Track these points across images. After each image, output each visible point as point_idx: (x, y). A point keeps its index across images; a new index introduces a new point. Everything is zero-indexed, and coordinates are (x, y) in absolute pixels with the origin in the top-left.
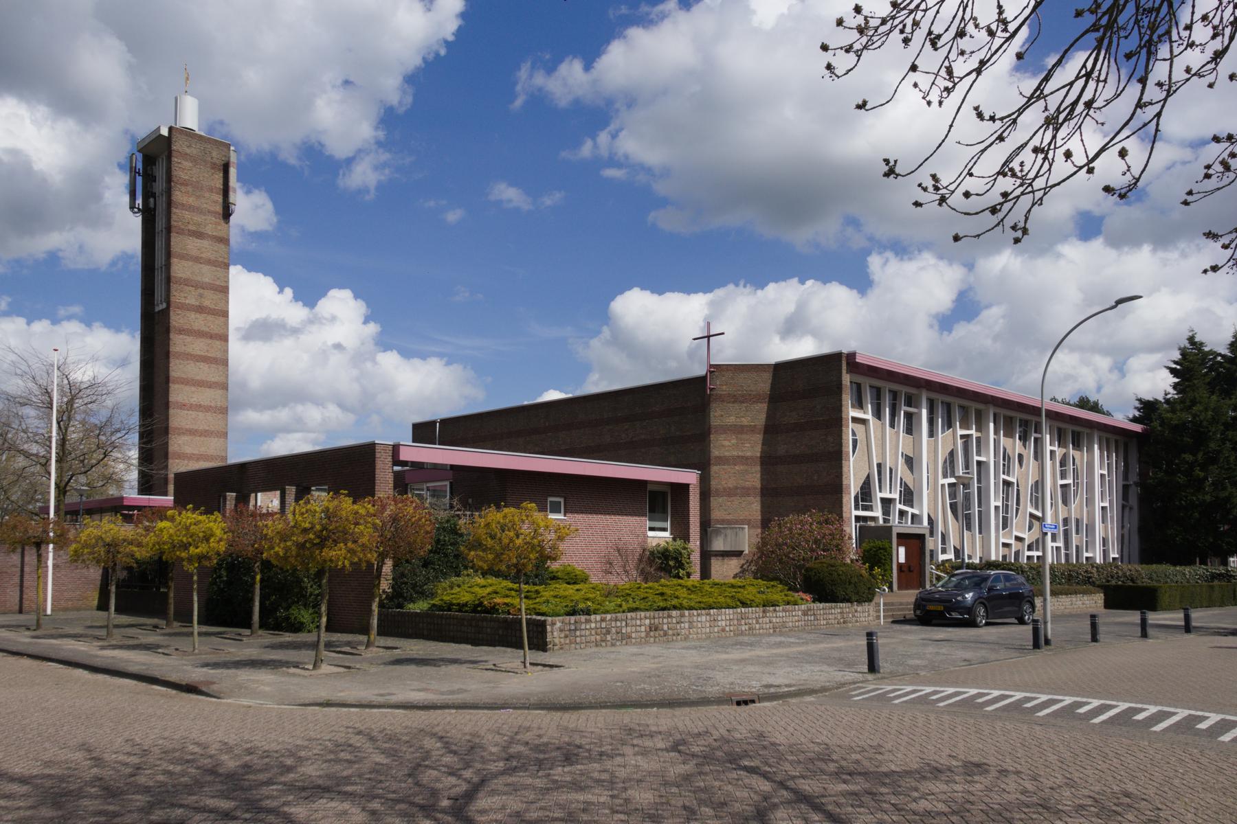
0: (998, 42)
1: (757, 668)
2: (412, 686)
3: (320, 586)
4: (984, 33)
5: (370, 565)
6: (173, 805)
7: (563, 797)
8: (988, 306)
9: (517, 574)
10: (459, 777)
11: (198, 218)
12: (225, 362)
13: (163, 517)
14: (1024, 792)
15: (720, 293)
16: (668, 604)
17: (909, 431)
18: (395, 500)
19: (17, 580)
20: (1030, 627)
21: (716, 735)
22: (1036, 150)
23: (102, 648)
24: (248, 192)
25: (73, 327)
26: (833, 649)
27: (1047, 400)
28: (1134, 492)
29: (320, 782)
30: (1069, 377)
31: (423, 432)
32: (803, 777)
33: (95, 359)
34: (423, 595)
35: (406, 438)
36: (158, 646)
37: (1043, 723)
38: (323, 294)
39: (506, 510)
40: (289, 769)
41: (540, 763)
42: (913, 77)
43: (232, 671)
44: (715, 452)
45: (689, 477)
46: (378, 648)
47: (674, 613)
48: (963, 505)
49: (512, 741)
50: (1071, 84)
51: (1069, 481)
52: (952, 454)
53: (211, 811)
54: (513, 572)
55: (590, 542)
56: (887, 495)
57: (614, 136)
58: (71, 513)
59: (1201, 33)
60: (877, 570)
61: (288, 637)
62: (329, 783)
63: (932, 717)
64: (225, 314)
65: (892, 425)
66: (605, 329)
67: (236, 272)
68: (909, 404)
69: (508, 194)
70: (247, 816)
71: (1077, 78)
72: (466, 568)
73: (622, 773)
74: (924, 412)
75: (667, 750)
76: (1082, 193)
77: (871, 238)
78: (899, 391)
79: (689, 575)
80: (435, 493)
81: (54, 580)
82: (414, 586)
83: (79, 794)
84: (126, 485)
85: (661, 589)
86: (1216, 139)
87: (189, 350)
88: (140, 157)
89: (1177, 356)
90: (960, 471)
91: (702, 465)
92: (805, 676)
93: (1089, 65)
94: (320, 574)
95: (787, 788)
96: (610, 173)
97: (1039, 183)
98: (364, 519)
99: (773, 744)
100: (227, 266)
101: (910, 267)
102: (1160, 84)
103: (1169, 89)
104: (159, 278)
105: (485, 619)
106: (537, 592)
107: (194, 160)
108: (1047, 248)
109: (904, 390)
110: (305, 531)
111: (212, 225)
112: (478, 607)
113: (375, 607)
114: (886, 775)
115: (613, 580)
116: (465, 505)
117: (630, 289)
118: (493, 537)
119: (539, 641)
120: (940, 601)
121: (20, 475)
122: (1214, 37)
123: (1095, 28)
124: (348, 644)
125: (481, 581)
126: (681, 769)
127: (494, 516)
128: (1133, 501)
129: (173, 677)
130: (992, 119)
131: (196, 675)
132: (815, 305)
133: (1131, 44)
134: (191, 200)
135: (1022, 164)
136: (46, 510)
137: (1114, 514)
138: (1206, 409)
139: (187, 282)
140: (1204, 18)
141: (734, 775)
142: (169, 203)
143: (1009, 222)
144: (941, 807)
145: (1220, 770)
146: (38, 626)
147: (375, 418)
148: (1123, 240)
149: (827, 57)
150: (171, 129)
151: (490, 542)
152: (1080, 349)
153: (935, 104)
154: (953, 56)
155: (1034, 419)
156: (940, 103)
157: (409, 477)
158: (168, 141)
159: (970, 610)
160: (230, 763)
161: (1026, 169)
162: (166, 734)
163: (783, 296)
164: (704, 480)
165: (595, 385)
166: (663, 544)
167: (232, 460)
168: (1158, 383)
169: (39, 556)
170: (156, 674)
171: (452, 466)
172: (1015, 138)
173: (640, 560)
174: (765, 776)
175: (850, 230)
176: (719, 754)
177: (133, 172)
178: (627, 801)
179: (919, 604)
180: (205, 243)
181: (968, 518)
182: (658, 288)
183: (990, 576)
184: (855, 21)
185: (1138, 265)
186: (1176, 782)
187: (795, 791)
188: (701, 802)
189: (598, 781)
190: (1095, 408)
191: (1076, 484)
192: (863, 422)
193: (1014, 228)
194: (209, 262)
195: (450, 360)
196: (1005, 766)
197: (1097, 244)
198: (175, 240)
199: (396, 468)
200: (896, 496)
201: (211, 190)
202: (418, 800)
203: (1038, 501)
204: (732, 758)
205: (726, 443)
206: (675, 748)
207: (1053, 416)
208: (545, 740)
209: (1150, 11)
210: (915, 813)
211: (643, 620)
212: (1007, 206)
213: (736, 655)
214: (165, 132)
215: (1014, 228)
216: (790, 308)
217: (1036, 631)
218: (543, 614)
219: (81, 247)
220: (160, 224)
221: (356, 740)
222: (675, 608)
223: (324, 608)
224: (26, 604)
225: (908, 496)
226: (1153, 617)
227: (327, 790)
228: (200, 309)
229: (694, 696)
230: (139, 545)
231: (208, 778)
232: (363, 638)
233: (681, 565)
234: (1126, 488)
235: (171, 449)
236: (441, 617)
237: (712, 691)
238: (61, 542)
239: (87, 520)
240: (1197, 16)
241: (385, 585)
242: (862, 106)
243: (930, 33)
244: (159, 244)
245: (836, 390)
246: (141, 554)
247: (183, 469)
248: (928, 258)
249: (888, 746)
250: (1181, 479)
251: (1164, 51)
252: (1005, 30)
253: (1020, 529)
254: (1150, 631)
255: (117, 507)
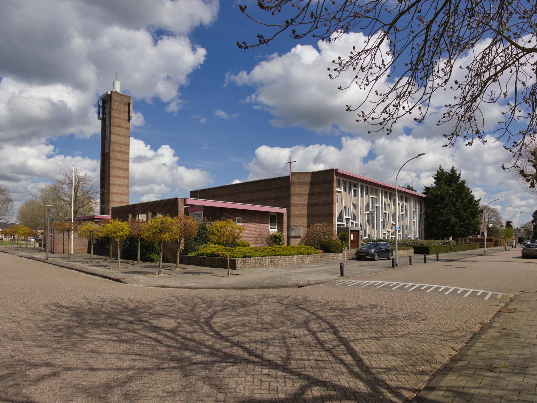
0: (382, 71)
1: (305, 275)
2: (191, 281)
3: (160, 247)
4: (378, 68)
5: (177, 240)
6: (114, 318)
7: (241, 318)
8: (379, 155)
9: (226, 244)
10: (207, 311)
11: (120, 121)
12: (128, 170)
13: (108, 223)
14: (388, 313)
15: (294, 148)
16: (276, 254)
17: (355, 196)
18: (185, 217)
19: (62, 242)
20: (391, 260)
21: (292, 297)
22: (394, 106)
23: (89, 266)
24: (136, 113)
25: (79, 158)
26: (330, 269)
27: (397, 186)
28: (423, 216)
29: (161, 312)
30: (403, 179)
31: (194, 194)
32: (319, 311)
33: (86, 169)
34: (195, 250)
35: (188, 196)
36: (107, 266)
37: (394, 291)
38: (160, 147)
39: (222, 222)
40: (151, 308)
41: (234, 307)
42: (356, 80)
43: (131, 275)
44: (292, 202)
45: (283, 210)
46: (179, 268)
47: (278, 257)
48: (371, 220)
49: (225, 300)
50: (404, 86)
51: (404, 213)
52: (368, 203)
53: (126, 321)
54: (225, 243)
55: (250, 233)
56: (347, 217)
57: (257, 96)
58: (79, 221)
59: (441, 74)
60: (344, 242)
61: (149, 264)
62: (164, 313)
63: (361, 290)
64: (128, 153)
65: (349, 194)
66: (254, 159)
67: (131, 139)
68: (355, 187)
69: (221, 113)
70: (138, 323)
71: (406, 84)
72: (209, 241)
73: (261, 310)
74: (360, 189)
75: (275, 303)
76: (405, 121)
77: (341, 132)
78: (352, 182)
79: (283, 244)
80: (198, 215)
81: (74, 243)
82: (191, 247)
83: (84, 313)
84: (96, 212)
85: (274, 249)
86: (446, 106)
87: (117, 165)
88: (101, 101)
89: (436, 173)
90: (371, 209)
91: (288, 206)
92: (320, 278)
93: (410, 80)
94: (160, 243)
95: (314, 314)
96: (256, 107)
97: (395, 116)
98: (174, 225)
99: (310, 300)
100: (129, 137)
101: (354, 141)
102: (430, 88)
103: (433, 89)
104: (107, 141)
105: (214, 259)
106: (233, 250)
107: (119, 102)
108: (396, 138)
109: (353, 182)
110: (155, 228)
111: (124, 124)
112: (213, 255)
113: (178, 254)
114: (346, 309)
115: (258, 246)
116: (208, 220)
117: (262, 145)
118: (218, 231)
119: (233, 266)
120: (364, 252)
121: (62, 207)
122: (445, 75)
123: (411, 69)
124: (169, 266)
125: (214, 246)
126: (280, 309)
127: (218, 224)
128: (423, 220)
129: (112, 277)
130: (381, 95)
131: (119, 276)
132: (324, 153)
133: (422, 75)
134: (118, 115)
135: (389, 110)
136: (70, 219)
137: (417, 224)
138: (444, 190)
139: (116, 143)
140: (442, 69)
141: (297, 310)
142: (110, 116)
143: (386, 128)
144: (363, 319)
145: (444, 303)
146: (69, 258)
147: (177, 189)
148: (417, 136)
149: (330, 72)
150: (111, 92)
151: (217, 233)
152: (406, 170)
153: (363, 89)
154: (369, 74)
155: (393, 192)
156: (364, 89)
157: (190, 209)
158: (110, 96)
159: (373, 255)
160: (131, 305)
161: (391, 111)
162: (111, 295)
163: (314, 150)
164: (289, 212)
165: (251, 178)
166: (275, 233)
167: (131, 203)
168: (430, 182)
169: (69, 235)
170: (107, 275)
171: (204, 206)
172: (387, 102)
173: (267, 239)
174: (307, 311)
175: (335, 129)
176: (292, 303)
177: (99, 106)
178: (262, 319)
179: (357, 253)
180: (122, 129)
181: (373, 225)
182: (271, 146)
183: (379, 244)
184: (338, 61)
185: (423, 144)
186: (432, 307)
187: (317, 315)
188: (287, 320)
189: (253, 313)
190: (412, 189)
191: (406, 214)
192: (340, 192)
193: (387, 130)
194: (123, 136)
195: (202, 169)
196: (383, 305)
197: (411, 137)
198: (112, 128)
199: (185, 207)
200: (350, 217)
201: (124, 112)
202: (194, 319)
203: (394, 219)
204: (297, 305)
205: (296, 199)
206: (278, 302)
207: (399, 191)
208: (235, 299)
209: (427, 66)
210: (354, 321)
211: (268, 259)
212: (385, 123)
213: (298, 271)
214: (109, 93)
215: (387, 130)
216: (316, 153)
217: (393, 262)
218: (235, 257)
219: (81, 132)
220: (107, 123)
221: (172, 299)
222: (278, 255)
223: (161, 255)
224: (65, 250)
225: (354, 217)
226: (428, 257)
227: (163, 315)
228: (120, 152)
229: (284, 285)
230: (100, 232)
231: (125, 310)
232: (175, 265)
233: (280, 241)
234: (421, 215)
235: (110, 199)
236: (200, 258)
237: (290, 283)
238: (76, 230)
239: (83, 223)
240: (440, 69)
241: (182, 247)
242: (340, 88)
243: (362, 67)
244: (107, 130)
245: (332, 181)
246: (101, 235)
247: (114, 206)
248: (360, 139)
249: (347, 300)
250: (437, 212)
251: (431, 78)
252: (385, 68)
253: (389, 228)
254: (427, 261)
255: (93, 219)
